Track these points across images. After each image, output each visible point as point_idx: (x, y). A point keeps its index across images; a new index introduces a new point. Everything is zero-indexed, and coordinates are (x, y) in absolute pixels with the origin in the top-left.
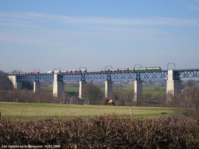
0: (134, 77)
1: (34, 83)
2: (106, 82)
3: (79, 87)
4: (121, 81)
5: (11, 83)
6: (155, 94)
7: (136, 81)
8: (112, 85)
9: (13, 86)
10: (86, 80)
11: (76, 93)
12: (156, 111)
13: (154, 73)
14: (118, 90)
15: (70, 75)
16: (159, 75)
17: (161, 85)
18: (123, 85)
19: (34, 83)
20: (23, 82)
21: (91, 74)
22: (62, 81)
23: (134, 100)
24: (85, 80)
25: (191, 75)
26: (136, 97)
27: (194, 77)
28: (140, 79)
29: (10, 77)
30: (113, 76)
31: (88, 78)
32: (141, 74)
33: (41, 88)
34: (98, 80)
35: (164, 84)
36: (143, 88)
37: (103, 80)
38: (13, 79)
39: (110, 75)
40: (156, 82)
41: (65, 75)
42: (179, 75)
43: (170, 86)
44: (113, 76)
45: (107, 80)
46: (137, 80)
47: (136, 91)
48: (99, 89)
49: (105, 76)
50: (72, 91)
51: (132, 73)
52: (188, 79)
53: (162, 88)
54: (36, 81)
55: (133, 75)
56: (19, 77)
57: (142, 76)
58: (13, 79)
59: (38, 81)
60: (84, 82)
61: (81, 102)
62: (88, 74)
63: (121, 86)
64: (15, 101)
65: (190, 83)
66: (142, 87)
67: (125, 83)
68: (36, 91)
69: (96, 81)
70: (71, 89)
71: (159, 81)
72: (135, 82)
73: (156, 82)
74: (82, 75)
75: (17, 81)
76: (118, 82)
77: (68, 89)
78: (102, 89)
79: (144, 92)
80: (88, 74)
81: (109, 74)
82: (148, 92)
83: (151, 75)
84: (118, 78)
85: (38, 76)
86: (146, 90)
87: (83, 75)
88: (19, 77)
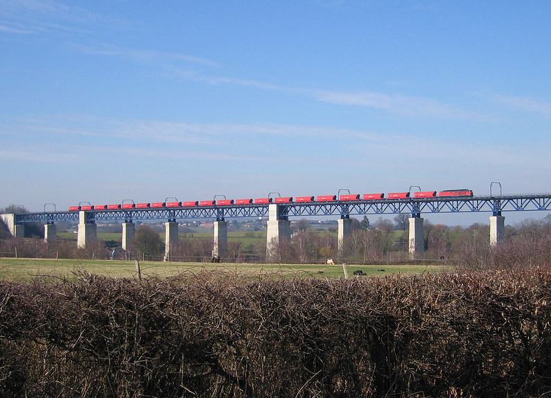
0: (214, 215)
1: (46, 226)
2: (167, 224)
3: (122, 232)
4: (187, 223)
5: (5, 226)
6: (246, 242)
7: (414, 219)
8: (177, 230)
9: (8, 230)
10: (133, 222)
11: (116, 242)
12: (425, 266)
13: (260, 209)
14: (185, 236)
15: (116, 212)
16: (254, 213)
17: (253, 229)
18: (190, 228)
19: (46, 226)
20: (26, 225)
21: (142, 211)
22: (93, 222)
23: (491, 241)
24: (131, 221)
25: (321, 212)
26: (216, 247)
27: (310, 214)
28: (223, 219)
29: (3, 216)
30: (178, 214)
31: (137, 218)
32: (225, 211)
33: (57, 234)
34: (149, 221)
35: (262, 225)
36: (229, 234)
37: (163, 220)
38: (10, 219)
39: (174, 213)
40: (244, 223)
41: (97, 213)
42: (93, 217)
43: (273, 230)
44: (178, 214)
45: (169, 221)
46: (218, 220)
47: (216, 240)
48: (158, 237)
49: (214, 214)
50: (110, 240)
51: (210, 209)
52: (299, 218)
53: (257, 233)
54: (48, 223)
55: (212, 211)
56: (20, 217)
57: (227, 214)
58: (10, 219)
59: (53, 223)
60: (130, 224)
61: (119, 255)
62: (137, 212)
63: (189, 231)
64: (14, 256)
65: (303, 225)
66: (226, 231)
67: (193, 225)
68: (48, 240)
69: (144, 220)
70: (112, 237)
71: (249, 222)
72: (216, 224)
73: (244, 223)
74: (129, 211)
75: (16, 223)
76: (182, 224)
77: (104, 236)
78: (161, 235)
79: (229, 240)
80: (137, 212)
81: (129, 213)
82: (236, 240)
83: (240, 213)
84: (186, 217)
85: (52, 215)
86: (233, 236)
87: (129, 213)
88: (20, 217)
